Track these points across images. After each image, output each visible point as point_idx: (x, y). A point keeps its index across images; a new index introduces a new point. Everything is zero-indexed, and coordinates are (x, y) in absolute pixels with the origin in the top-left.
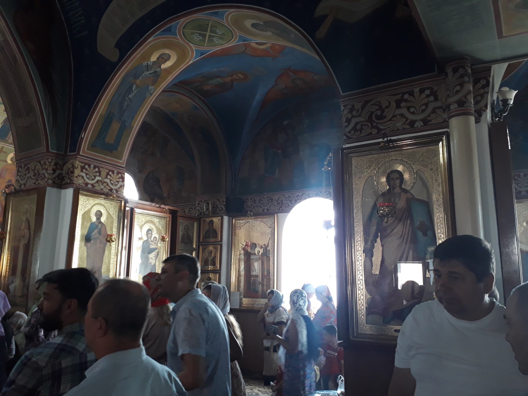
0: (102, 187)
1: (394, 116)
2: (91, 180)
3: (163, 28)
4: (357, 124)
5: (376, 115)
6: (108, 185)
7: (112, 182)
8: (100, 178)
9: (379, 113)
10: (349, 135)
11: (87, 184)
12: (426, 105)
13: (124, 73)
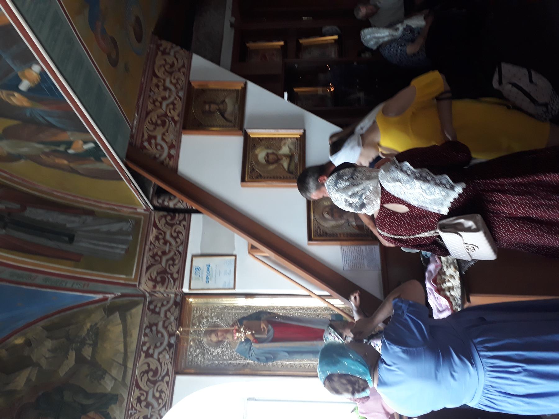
0: (172, 318)
1: (159, 360)
2: (164, 338)
3: (108, 83)
6: (169, 310)
7: (158, 344)
8: (161, 324)
9: (151, 374)
10: (161, 406)
11: (170, 345)
12: (158, 332)
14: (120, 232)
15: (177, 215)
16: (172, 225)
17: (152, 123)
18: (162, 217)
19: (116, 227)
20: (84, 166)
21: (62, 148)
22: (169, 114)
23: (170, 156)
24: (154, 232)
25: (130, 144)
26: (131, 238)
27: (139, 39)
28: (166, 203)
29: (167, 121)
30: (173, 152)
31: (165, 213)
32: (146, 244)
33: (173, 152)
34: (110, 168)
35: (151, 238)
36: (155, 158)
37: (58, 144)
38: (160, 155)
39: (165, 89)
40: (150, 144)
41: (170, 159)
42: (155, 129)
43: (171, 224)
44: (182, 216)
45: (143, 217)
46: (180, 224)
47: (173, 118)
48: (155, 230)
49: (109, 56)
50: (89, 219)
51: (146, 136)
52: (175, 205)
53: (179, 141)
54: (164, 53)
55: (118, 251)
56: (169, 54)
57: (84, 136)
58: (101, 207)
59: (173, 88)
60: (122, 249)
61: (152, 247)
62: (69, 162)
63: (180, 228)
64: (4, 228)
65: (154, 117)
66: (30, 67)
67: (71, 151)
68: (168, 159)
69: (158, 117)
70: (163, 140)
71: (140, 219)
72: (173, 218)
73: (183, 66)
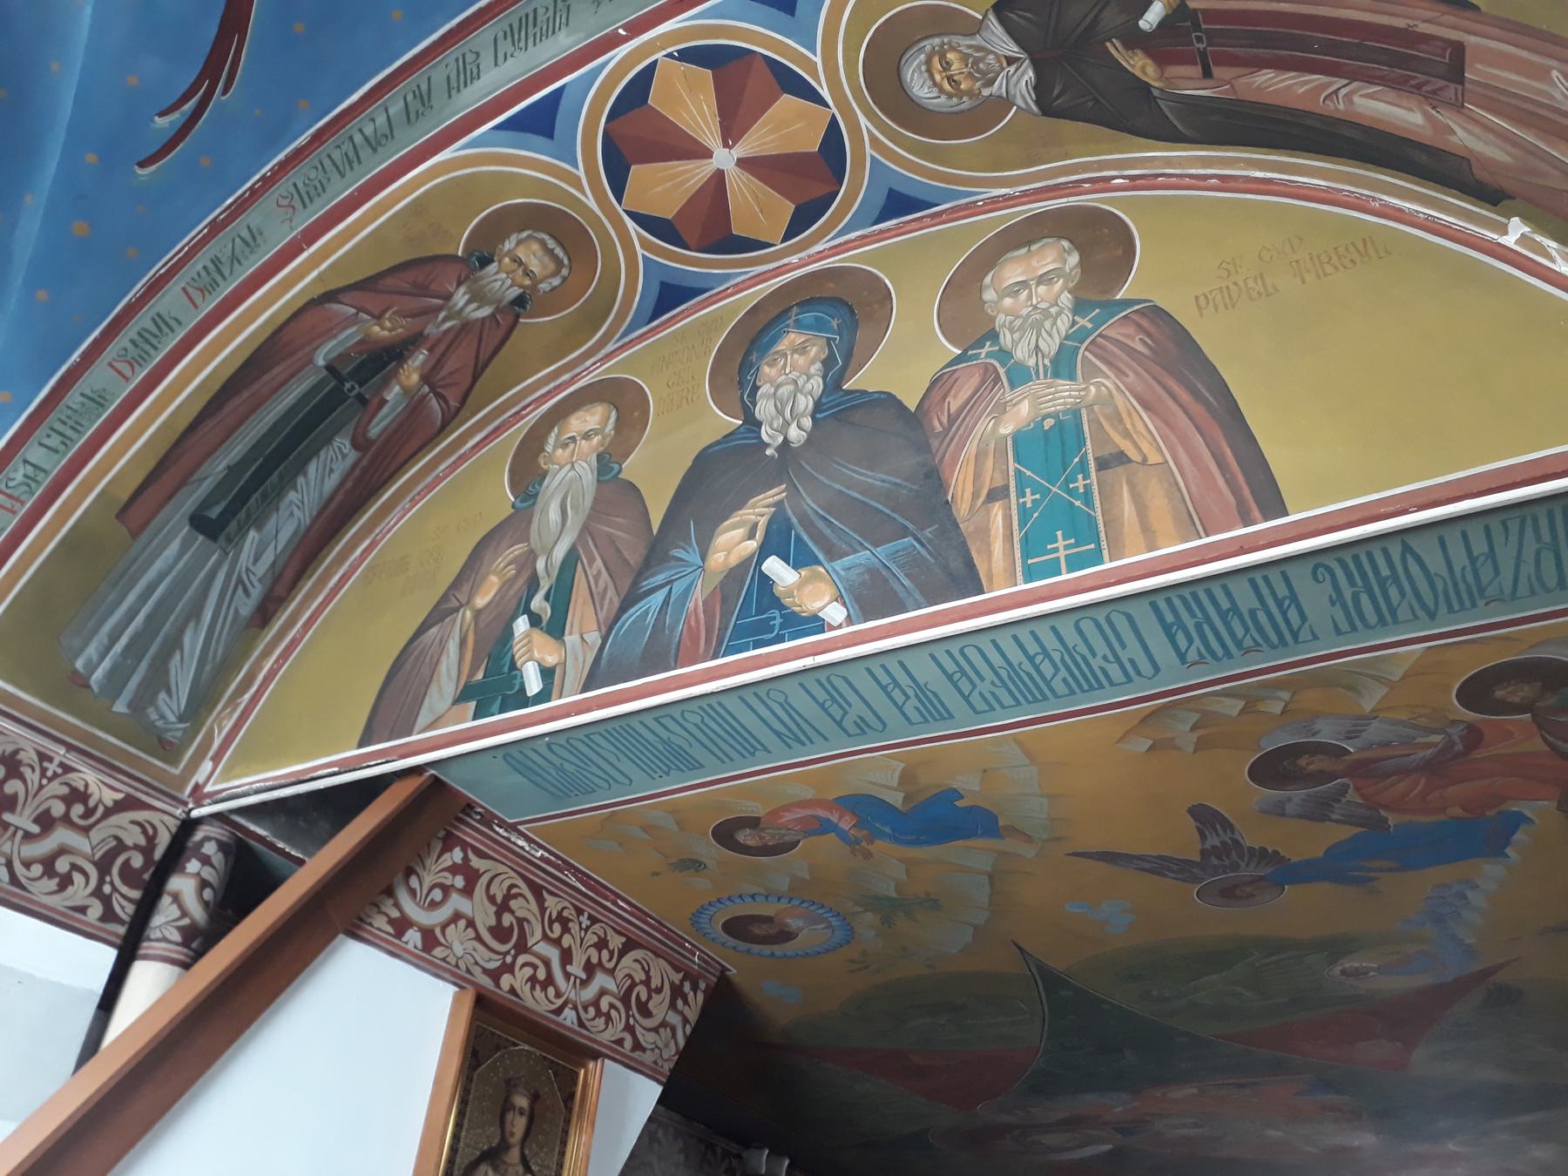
4: (62, 851)
5: (127, 863)
10: (19, 869)
13: (139, 286)
14: (158, 680)
15: (136, 894)
16: (104, 866)
17: (508, 897)
18: (151, 841)
19: (182, 675)
20: (453, 646)
21: (538, 603)
22: (521, 959)
23: (402, 925)
24: (103, 790)
25: (469, 807)
26: (120, 707)
27: (737, 928)
28: (193, 866)
29: (503, 948)
30: (413, 938)
31: (158, 854)
32: (70, 748)
33: (413, 938)
34: (422, 720)
35: (88, 777)
36: (410, 872)
37: (561, 597)
38: (413, 892)
39: (590, 968)
40: (454, 869)
41: (391, 921)
42: (492, 899)
43: (111, 863)
44: (124, 910)
45: (176, 771)
46: (97, 893)
47: (509, 969)
48: (109, 797)
49: (753, 823)
50: (246, 606)
51: (476, 862)
52: (176, 898)
53: (438, 970)
54: (677, 992)
55: (92, 650)
56: (673, 1006)
57: (575, 672)
58: (266, 653)
59: (589, 993)
60: (92, 668)
61: (52, 768)
62: (478, 614)
63: (80, 891)
64: (330, 368)
65: (525, 906)
66: (839, 598)
67: (522, 625)
68: (395, 914)
69: (521, 921)
70: (456, 917)
71: (174, 762)
72: (128, 874)
73: (637, 1046)
